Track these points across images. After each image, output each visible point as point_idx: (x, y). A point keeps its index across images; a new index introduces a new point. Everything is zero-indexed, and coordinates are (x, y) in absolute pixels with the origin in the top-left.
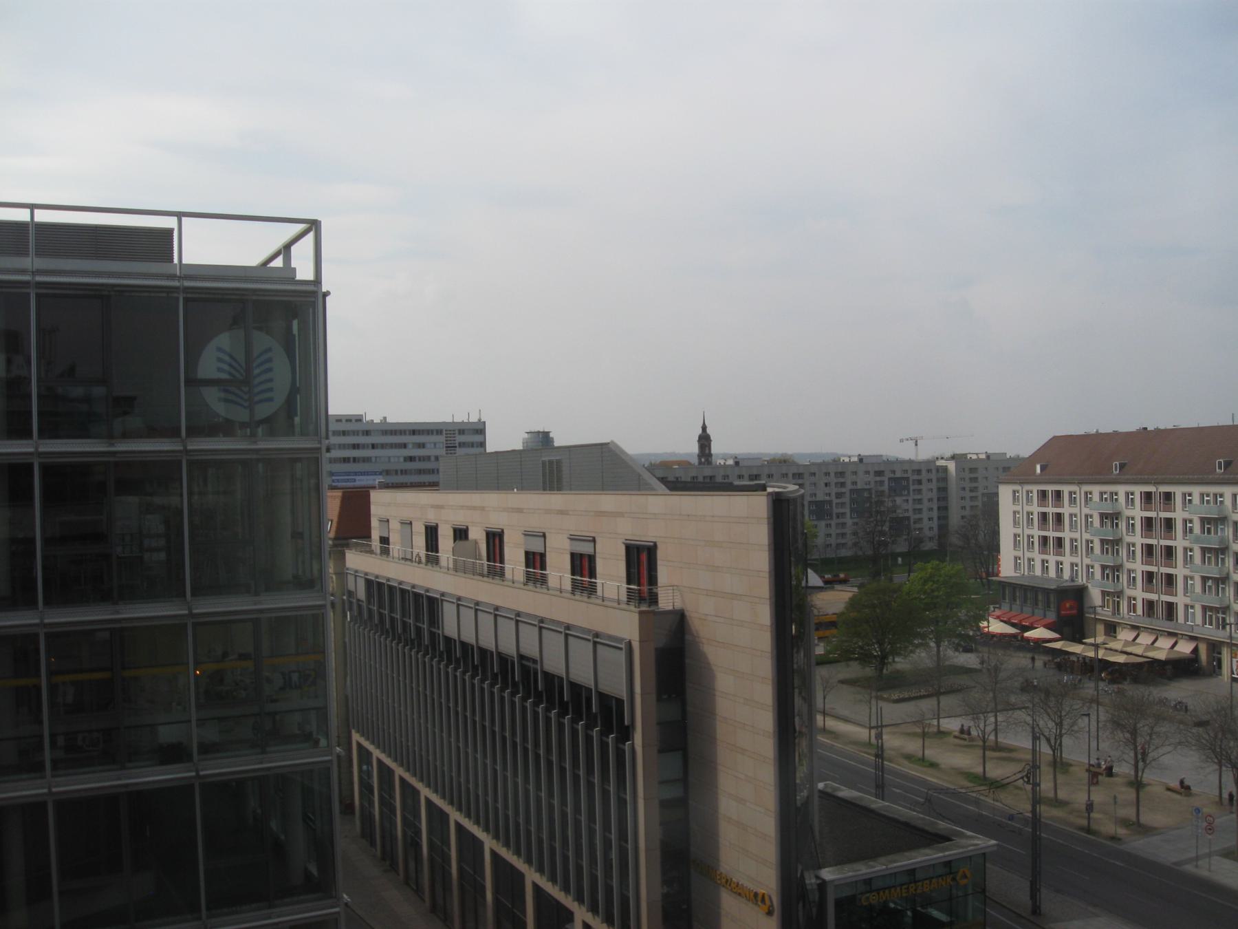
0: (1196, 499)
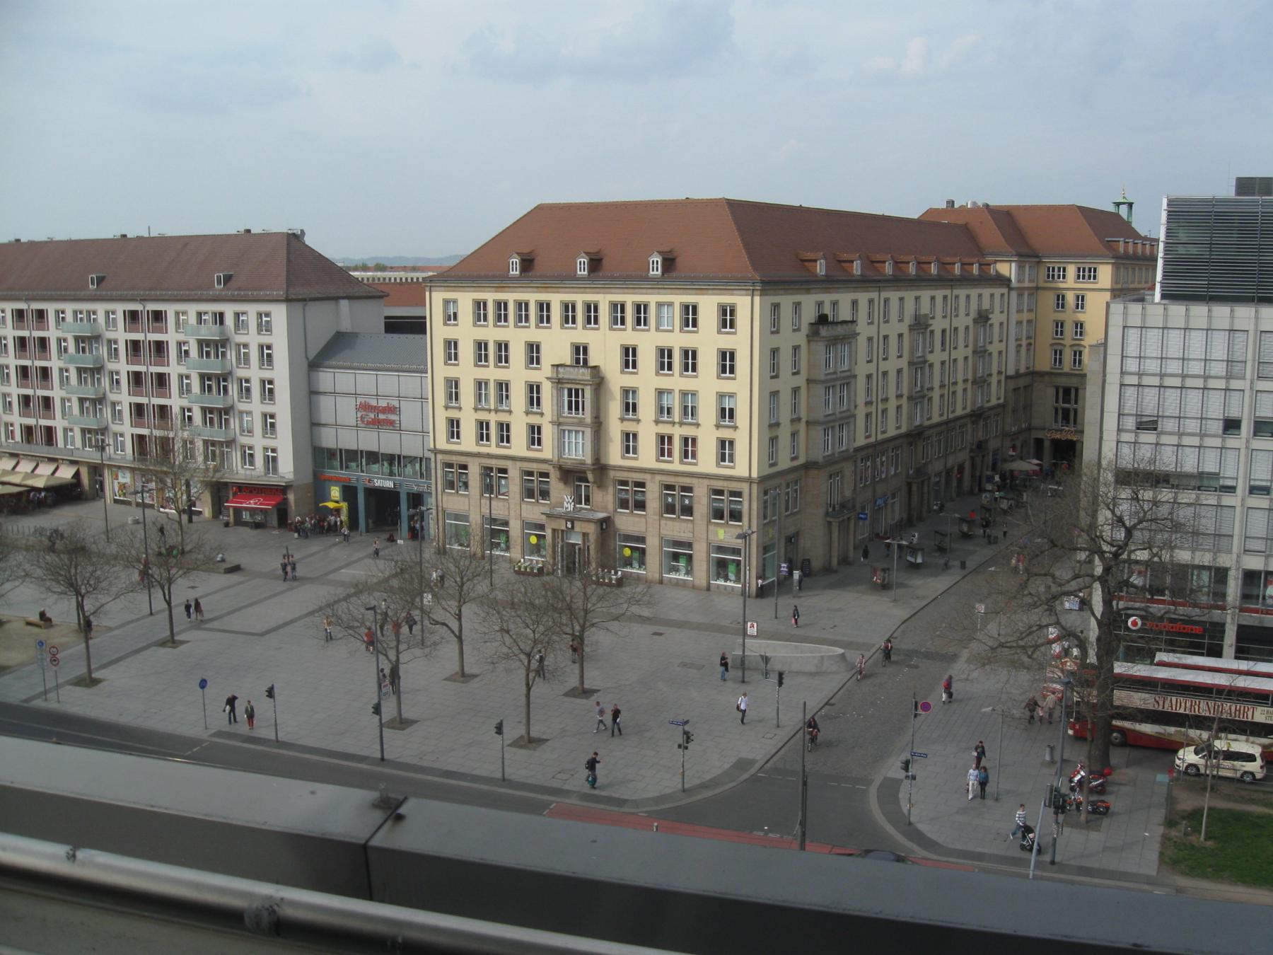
0: (69, 317)
